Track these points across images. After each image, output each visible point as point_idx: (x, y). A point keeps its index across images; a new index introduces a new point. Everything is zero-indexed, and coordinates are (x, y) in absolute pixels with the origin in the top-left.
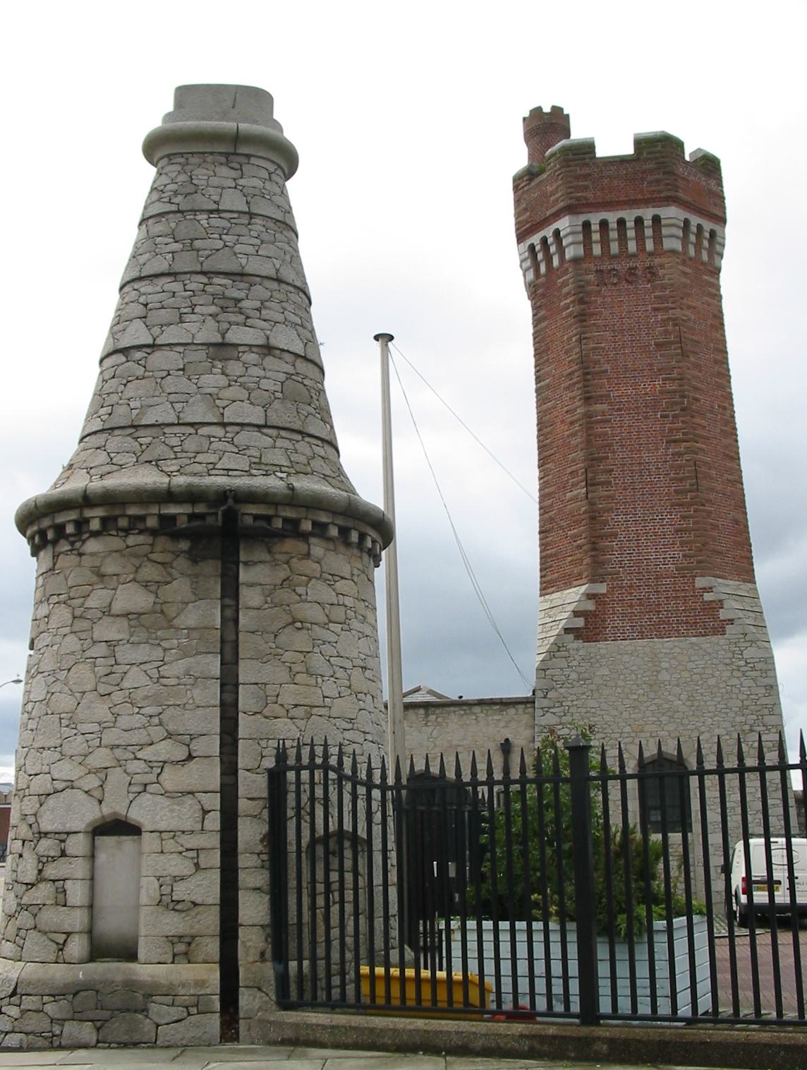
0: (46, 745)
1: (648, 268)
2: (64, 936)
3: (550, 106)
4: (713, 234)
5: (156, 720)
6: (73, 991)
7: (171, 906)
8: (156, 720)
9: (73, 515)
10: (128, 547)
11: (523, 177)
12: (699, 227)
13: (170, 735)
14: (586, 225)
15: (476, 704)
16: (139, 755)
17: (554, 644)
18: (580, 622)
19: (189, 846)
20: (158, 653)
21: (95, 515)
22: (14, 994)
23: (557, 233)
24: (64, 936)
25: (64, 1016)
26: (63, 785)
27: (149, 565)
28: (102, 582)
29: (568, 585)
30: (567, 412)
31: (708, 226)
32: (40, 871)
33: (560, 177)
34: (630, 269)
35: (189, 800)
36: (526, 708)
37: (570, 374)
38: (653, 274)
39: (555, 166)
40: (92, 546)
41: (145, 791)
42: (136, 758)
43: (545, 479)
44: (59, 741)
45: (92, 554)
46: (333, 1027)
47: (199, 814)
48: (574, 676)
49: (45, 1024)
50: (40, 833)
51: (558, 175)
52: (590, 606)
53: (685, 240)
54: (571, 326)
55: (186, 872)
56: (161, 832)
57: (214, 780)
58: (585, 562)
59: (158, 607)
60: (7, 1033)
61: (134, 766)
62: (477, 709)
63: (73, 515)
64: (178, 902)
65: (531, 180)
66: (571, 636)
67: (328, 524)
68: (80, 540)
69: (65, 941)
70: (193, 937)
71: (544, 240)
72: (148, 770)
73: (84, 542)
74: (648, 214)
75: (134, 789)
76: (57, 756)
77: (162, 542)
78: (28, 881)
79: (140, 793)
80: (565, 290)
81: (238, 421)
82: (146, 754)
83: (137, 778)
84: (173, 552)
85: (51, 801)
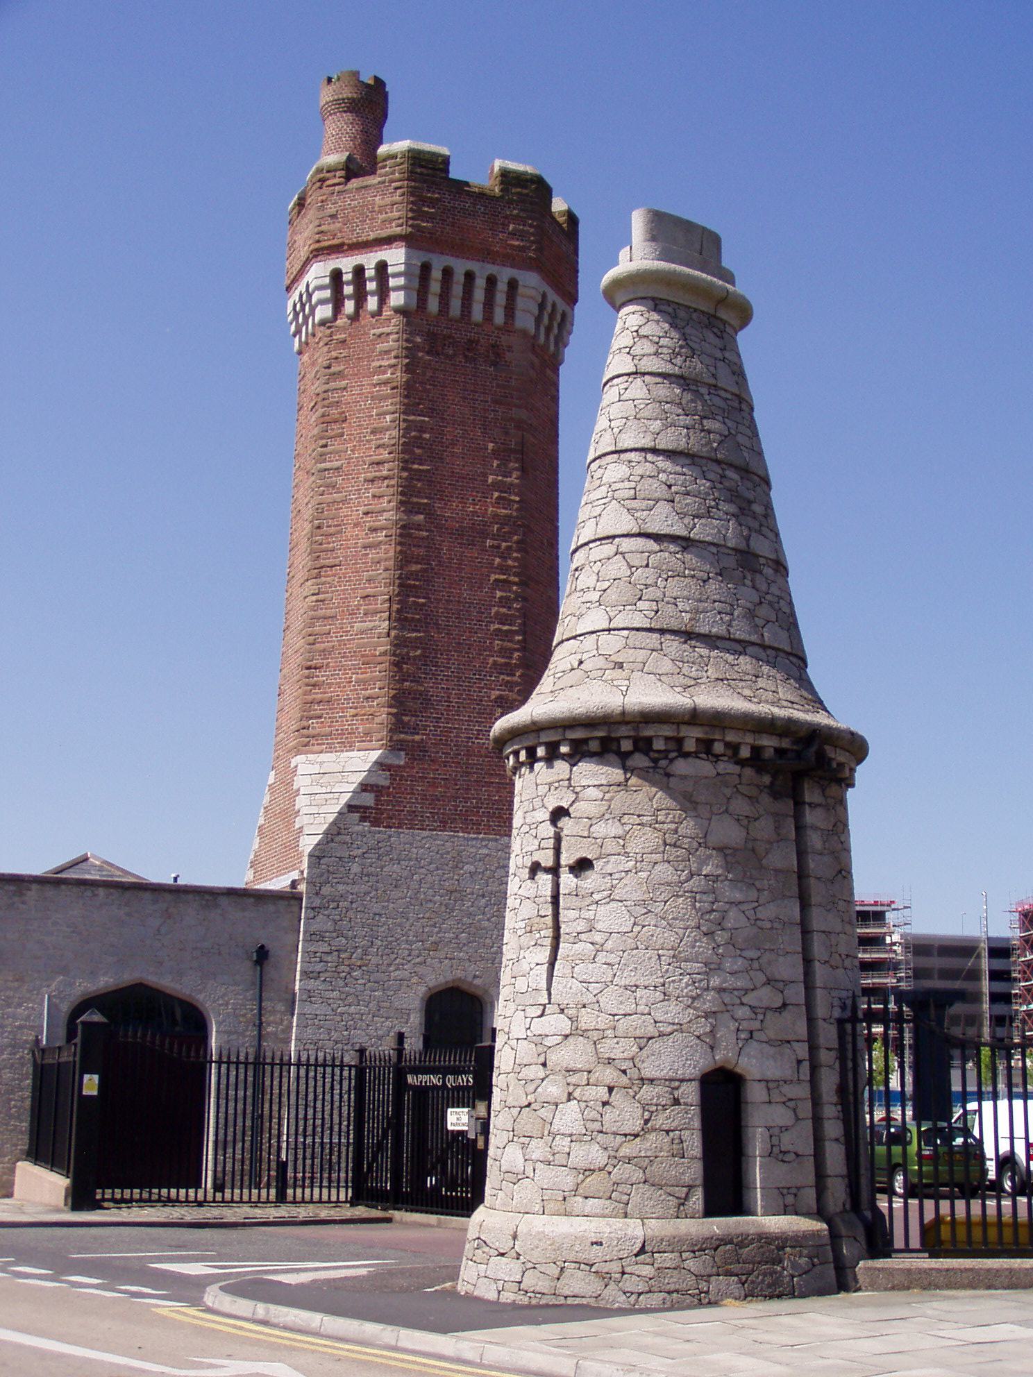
0: (641, 982)
1: (493, 346)
2: (685, 1189)
3: (372, 75)
4: (564, 315)
5: (756, 965)
6: (700, 1247)
7: (781, 1156)
8: (756, 965)
9: (668, 731)
10: (718, 774)
11: (335, 170)
12: (554, 306)
13: (769, 982)
14: (426, 268)
15: (223, 894)
16: (745, 1000)
17: (334, 823)
18: (368, 799)
19: (790, 1096)
20: (753, 894)
21: (692, 735)
22: (642, 1251)
23: (382, 267)
24: (685, 1189)
25: (709, 1271)
26: (670, 1029)
27: (740, 797)
28: (695, 809)
29: (350, 747)
30: (366, 514)
31: (561, 305)
32: (646, 1122)
33: (399, 191)
34: (469, 340)
35: (786, 1050)
36: (289, 905)
37: (378, 464)
38: (498, 355)
39: (393, 173)
40: (681, 767)
41: (751, 1038)
42: (742, 1004)
43: (321, 597)
44: (661, 980)
45: (684, 778)
46: (948, 1270)
47: (795, 1064)
48: (356, 868)
49: (691, 1281)
50: (642, 1079)
51: (396, 188)
52: (383, 780)
53: (538, 320)
54: (385, 398)
55: (789, 1123)
56: (767, 1081)
57: (802, 1029)
58: (377, 720)
59: (750, 846)
60: (640, 1294)
61: (742, 1012)
62: (101, 892)
63: (668, 731)
64: (785, 1153)
65: (348, 178)
66: (357, 815)
67: (740, 744)
68: (666, 758)
69: (687, 1194)
70: (798, 1188)
71: (359, 271)
72: (753, 1016)
73: (672, 761)
74: (505, 274)
75: (743, 1036)
76: (659, 996)
77: (748, 772)
78: (627, 1132)
79: (566, 1036)
80: (380, 347)
81: (776, 645)
82: (749, 999)
83: (745, 1025)
84: (758, 786)
85: (655, 1045)
